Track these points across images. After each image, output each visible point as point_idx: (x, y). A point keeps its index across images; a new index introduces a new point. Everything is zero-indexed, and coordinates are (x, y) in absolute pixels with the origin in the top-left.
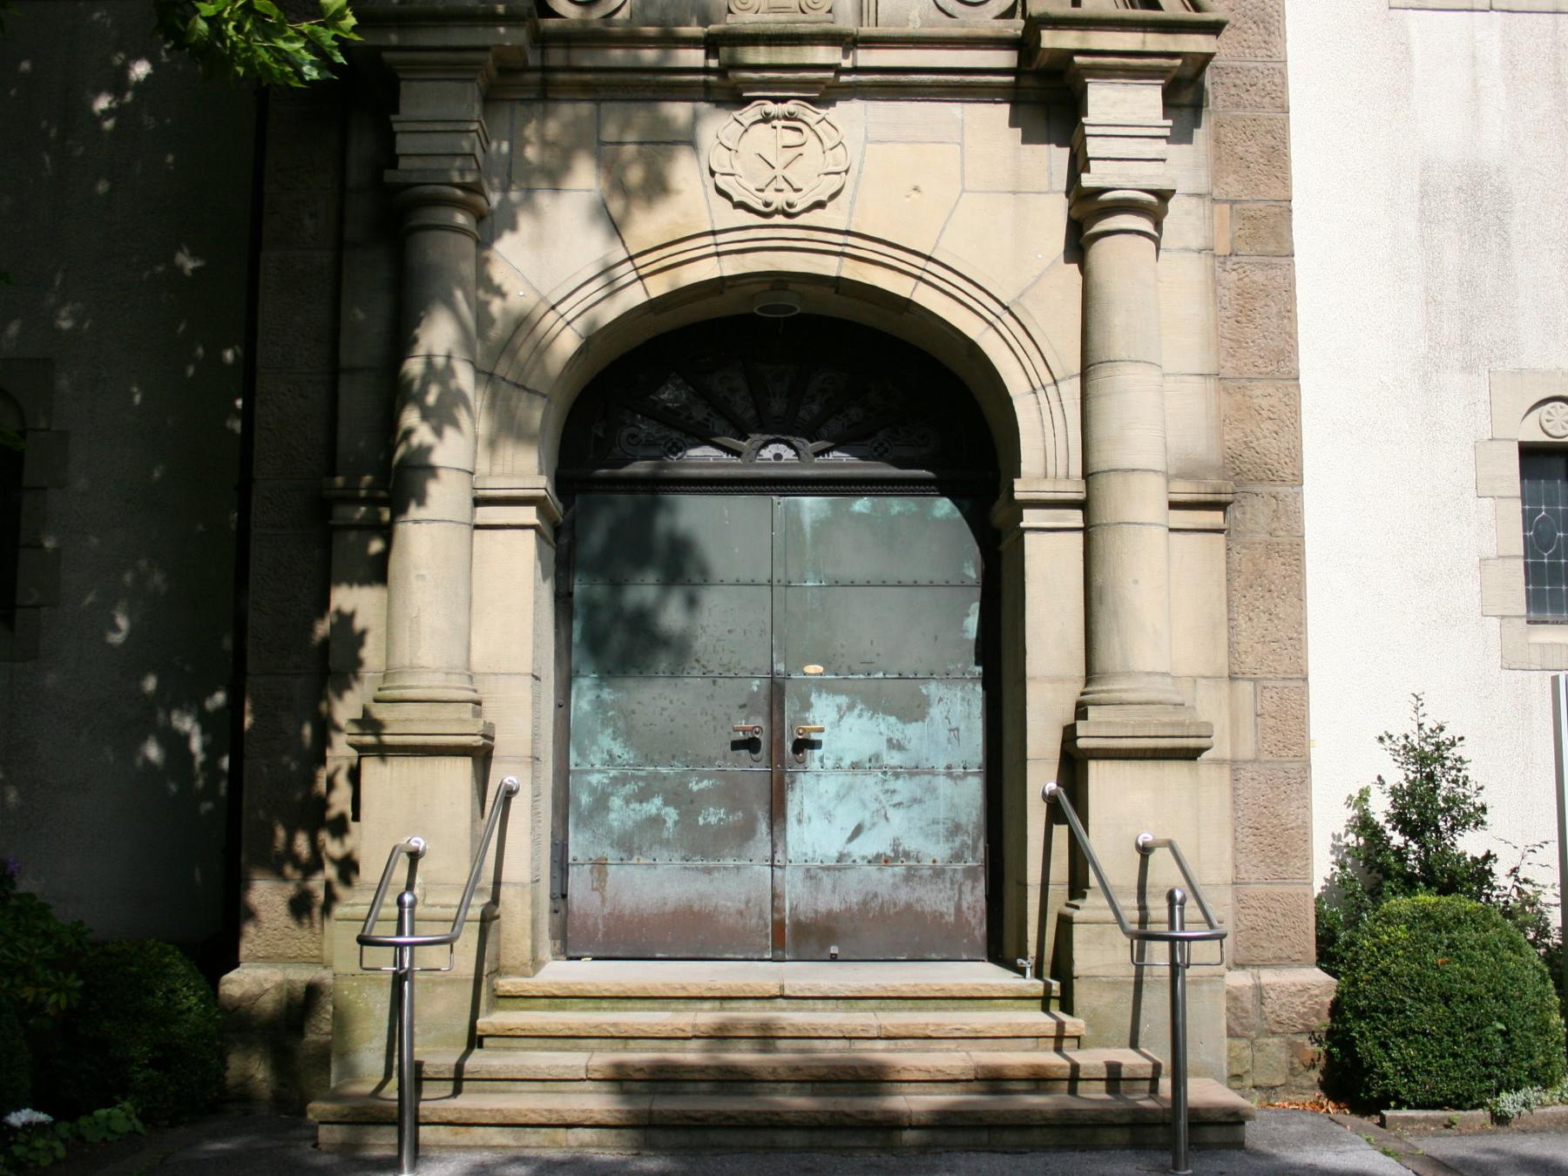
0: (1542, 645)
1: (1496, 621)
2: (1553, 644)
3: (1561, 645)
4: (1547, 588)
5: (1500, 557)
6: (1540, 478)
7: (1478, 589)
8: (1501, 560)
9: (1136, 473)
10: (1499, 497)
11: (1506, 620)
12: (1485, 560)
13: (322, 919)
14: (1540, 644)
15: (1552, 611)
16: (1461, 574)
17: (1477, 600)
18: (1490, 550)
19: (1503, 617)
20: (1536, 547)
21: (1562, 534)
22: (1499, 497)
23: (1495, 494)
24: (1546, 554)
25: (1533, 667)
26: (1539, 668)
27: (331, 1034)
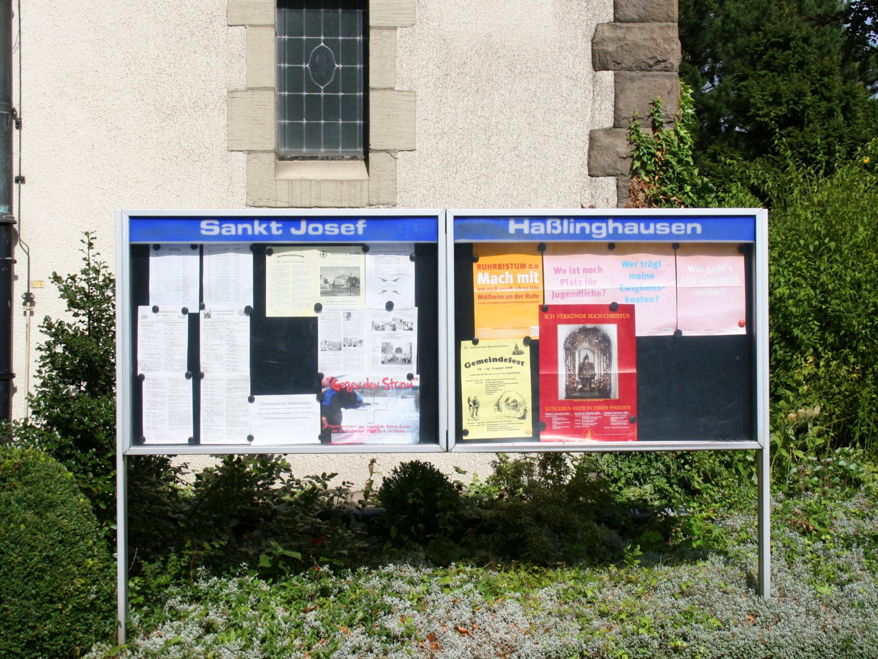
0: (290, 182)
1: (242, 156)
2: (302, 180)
3: (311, 181)
4: (323, 122)
5: (248, 89)
6: (300, 7)
7: (224, 123)
8: (250, 92)
9: (621, 105)
10: (251, 26)
11: (253, 155)
12: (331, 107)
13: (343, 432)
14: (288, 180)
15: (325, 148)
16: (206, 106)
17: (223, 135)
18: (240, 81)
19: (249, 152)
20: (312, 79)
21: (304, 66)
22: (251, 26)
23: (247, 22)
24: (322, 88)
25: (280, 204)
26: (287, 205)
27: (633, 484)
